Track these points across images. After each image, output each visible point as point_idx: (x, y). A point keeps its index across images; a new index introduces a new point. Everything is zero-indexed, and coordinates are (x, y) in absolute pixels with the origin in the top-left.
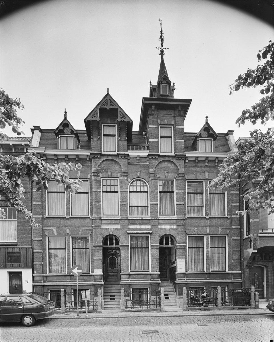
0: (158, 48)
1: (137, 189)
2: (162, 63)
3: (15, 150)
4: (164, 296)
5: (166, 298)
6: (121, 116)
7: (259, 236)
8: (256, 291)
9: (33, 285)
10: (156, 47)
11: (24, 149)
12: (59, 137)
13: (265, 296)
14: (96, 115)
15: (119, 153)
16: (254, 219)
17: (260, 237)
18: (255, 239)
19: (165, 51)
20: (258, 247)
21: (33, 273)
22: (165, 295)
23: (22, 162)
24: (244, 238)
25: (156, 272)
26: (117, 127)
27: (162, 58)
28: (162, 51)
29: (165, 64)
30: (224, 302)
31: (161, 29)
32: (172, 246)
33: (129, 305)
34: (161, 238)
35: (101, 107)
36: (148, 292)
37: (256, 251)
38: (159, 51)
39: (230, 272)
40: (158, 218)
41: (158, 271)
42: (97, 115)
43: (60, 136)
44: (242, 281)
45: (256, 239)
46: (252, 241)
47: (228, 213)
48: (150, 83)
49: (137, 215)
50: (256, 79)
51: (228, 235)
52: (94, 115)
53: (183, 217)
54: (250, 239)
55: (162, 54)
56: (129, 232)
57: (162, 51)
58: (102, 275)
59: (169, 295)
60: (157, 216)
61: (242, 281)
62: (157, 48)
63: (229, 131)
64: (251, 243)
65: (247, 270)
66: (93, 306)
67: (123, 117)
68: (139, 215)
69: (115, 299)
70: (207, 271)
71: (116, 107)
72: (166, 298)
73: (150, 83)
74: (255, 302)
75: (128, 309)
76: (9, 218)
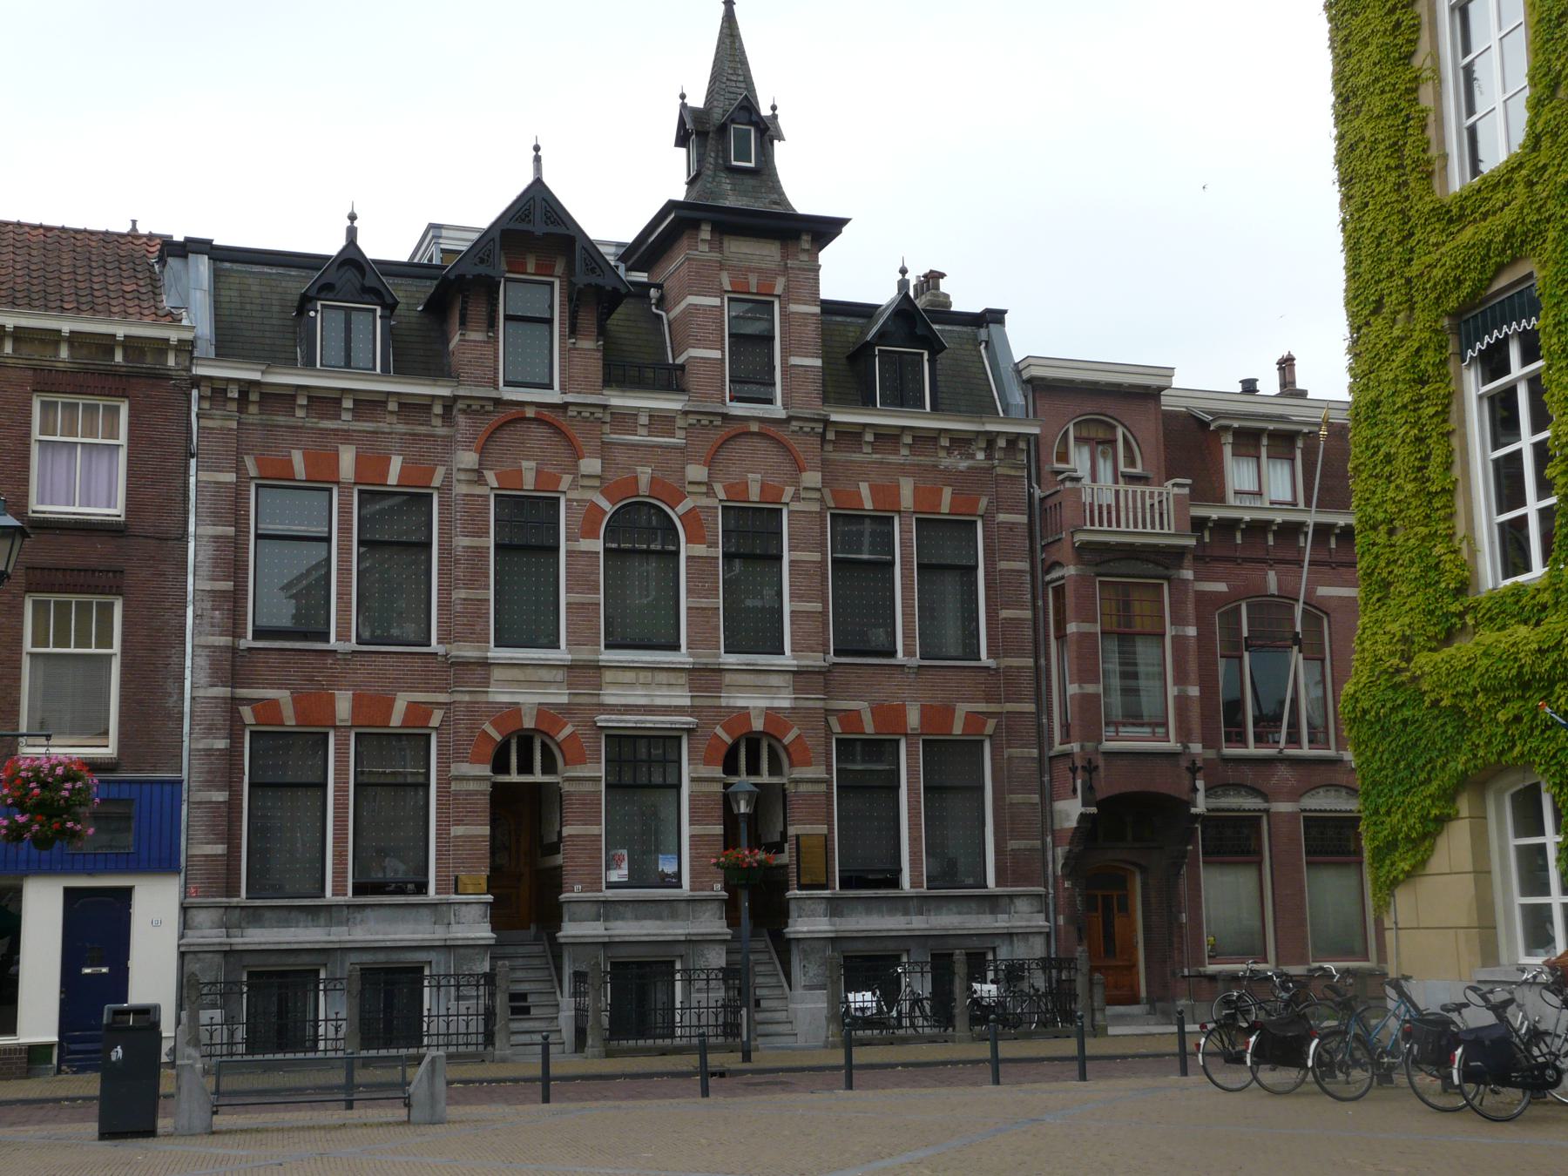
3: (125, 357)
4: (511, 1000)
5: (515, 1011)
7: (1104, 753)
8: (1093, 969)
9: (183, 949)
11: (167, 354)
12: (316, 311)
13: (1143, 993)
14: (488, 256)
15: (569, 398)
16: (1084, 685)
18: (1090, 761)
20: (1100, 796)
21: (186, 894)
22: (514, 997)
24: (1052, 754)
30: (385, 369)
32: (775, 780)
33: (690, 1027)
35: (508, 227)
37: (1093, 810)
39: (1000, 891)
41: (718, 886)
42: (491, 256)
43: (319, 308)
45: (1094, 764)
46: (1079, 771)
48: (683, 96)
52: (481, 255)
53: (818, 663)
54: (1073, 764)
56: (603, 720)
59: (530, 999)
60: (718, 656)
63: (988, 311)
64: (1074, 779)
65: (1067, 885)
67: (593, 270)
69: (533, 1011)
70: (911, 887)
71: (567, 232)
72: (515, 1011)
73: (683, 96)
74: (1093, 1010)
76: (96, 648)
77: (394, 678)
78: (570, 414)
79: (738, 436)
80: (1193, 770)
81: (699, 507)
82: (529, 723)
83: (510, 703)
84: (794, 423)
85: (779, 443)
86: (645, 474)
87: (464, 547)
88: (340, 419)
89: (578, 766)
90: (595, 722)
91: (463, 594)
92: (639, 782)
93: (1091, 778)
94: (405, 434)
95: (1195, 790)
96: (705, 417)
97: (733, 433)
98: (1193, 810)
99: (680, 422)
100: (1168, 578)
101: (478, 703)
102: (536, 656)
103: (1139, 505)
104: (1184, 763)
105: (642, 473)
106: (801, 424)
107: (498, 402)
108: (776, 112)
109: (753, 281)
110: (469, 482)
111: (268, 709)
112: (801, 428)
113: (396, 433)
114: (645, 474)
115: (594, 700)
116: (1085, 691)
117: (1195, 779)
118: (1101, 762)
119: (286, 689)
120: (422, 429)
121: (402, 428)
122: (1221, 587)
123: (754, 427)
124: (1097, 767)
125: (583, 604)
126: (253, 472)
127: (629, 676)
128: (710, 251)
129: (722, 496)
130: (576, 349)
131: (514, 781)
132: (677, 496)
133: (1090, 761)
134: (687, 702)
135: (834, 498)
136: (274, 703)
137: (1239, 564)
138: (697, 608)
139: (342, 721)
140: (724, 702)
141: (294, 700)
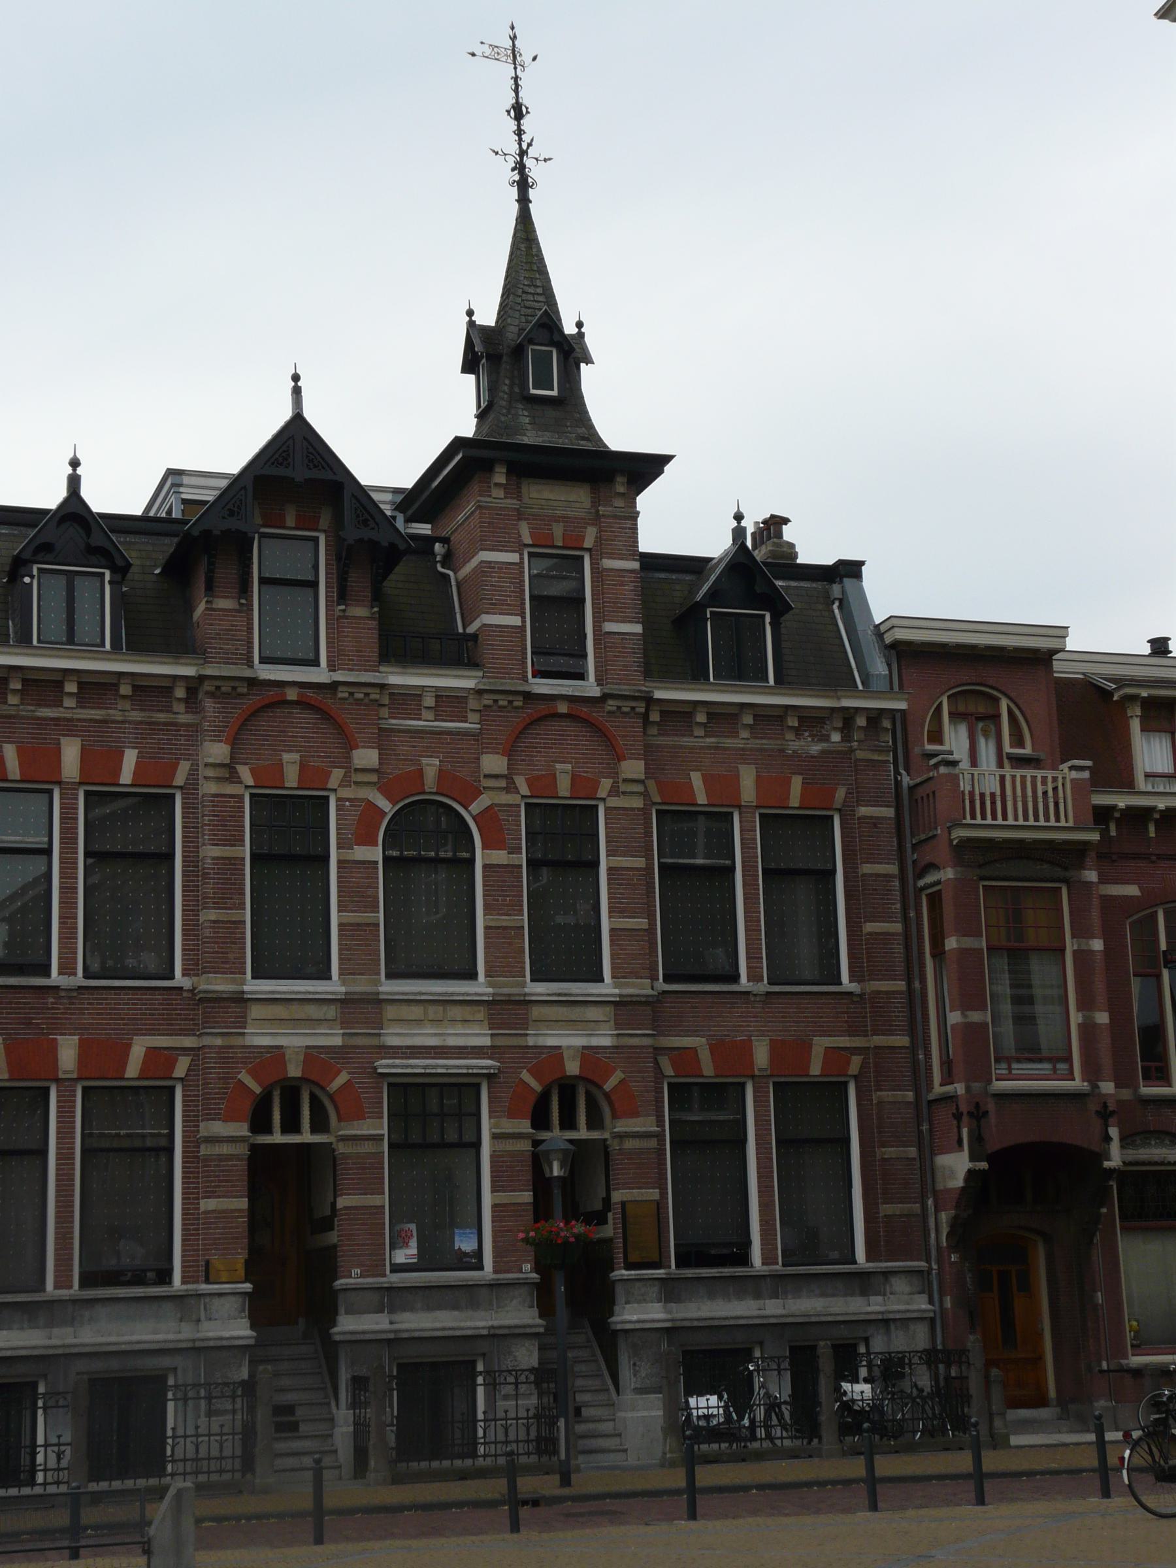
2: (525, 222)
6: (358, 516)
12: (32, 577)
13: (1052, 1393)
14: (239, 507)
15: (339, 676)
17: (1002, 1097)
18: (977, 1105)
19: (534, 170)
24: (931, 1097)
25: (521, 1272)
26: (327, 545)
27: (524, 201)
28: (520, 167)
29: (593, 421)
31: (516, 91)
32: (595, 1135)
36: (36, 1404)
37: (984, 1165)
40: (525, 995)
41: (527, 1267)
43: (35, 572)
44: (934, 1312)
46: (965, 1119)
48: (470, 313)
51: (839, 810)
54: (957, 1108)
55: (523, 185)
56: (385, 1065)
58: (246, 1293)
60: (524, 985)
61: (932, 1315)
62: (497, 153)
64: (959, 1128)
66: (209, 1459)
67: (365, 523)
70: (763, 1264)
73: (470, 313)
75: (900, 1355)
78: (340, 695)
80: (1105, 1115)
81: (496, 805)
84: (610, 702)
86: (431, 766)
92: (919, 1212)
93: (979, 1127)
94: (141, 723)
95: (1108, 1139)
98: (1106, 1164)
99: (473, 703)
100: (1066, 881)
102: (302, 989)
103: (1020, 805)
104: (1093, 1106)
105: (428, 765)
109: (558, 531)
110: (219, 779)
114: (431, 766)
115: (374, 1041)
116: (969, 1020)
117: (1107, 1126)
118: (991, 1106)
120: (162, 717)
121: (136, 715)
122: (1132, 890)
123: (563, 708)
124: (986, 1113)
125: (358, 924)
127: (416, 1012)
129: (524, 790)
130: (347, 617)
132: (470, 793)
133: (977, 1105)
137: (1153, 862)
138: (498, 928)
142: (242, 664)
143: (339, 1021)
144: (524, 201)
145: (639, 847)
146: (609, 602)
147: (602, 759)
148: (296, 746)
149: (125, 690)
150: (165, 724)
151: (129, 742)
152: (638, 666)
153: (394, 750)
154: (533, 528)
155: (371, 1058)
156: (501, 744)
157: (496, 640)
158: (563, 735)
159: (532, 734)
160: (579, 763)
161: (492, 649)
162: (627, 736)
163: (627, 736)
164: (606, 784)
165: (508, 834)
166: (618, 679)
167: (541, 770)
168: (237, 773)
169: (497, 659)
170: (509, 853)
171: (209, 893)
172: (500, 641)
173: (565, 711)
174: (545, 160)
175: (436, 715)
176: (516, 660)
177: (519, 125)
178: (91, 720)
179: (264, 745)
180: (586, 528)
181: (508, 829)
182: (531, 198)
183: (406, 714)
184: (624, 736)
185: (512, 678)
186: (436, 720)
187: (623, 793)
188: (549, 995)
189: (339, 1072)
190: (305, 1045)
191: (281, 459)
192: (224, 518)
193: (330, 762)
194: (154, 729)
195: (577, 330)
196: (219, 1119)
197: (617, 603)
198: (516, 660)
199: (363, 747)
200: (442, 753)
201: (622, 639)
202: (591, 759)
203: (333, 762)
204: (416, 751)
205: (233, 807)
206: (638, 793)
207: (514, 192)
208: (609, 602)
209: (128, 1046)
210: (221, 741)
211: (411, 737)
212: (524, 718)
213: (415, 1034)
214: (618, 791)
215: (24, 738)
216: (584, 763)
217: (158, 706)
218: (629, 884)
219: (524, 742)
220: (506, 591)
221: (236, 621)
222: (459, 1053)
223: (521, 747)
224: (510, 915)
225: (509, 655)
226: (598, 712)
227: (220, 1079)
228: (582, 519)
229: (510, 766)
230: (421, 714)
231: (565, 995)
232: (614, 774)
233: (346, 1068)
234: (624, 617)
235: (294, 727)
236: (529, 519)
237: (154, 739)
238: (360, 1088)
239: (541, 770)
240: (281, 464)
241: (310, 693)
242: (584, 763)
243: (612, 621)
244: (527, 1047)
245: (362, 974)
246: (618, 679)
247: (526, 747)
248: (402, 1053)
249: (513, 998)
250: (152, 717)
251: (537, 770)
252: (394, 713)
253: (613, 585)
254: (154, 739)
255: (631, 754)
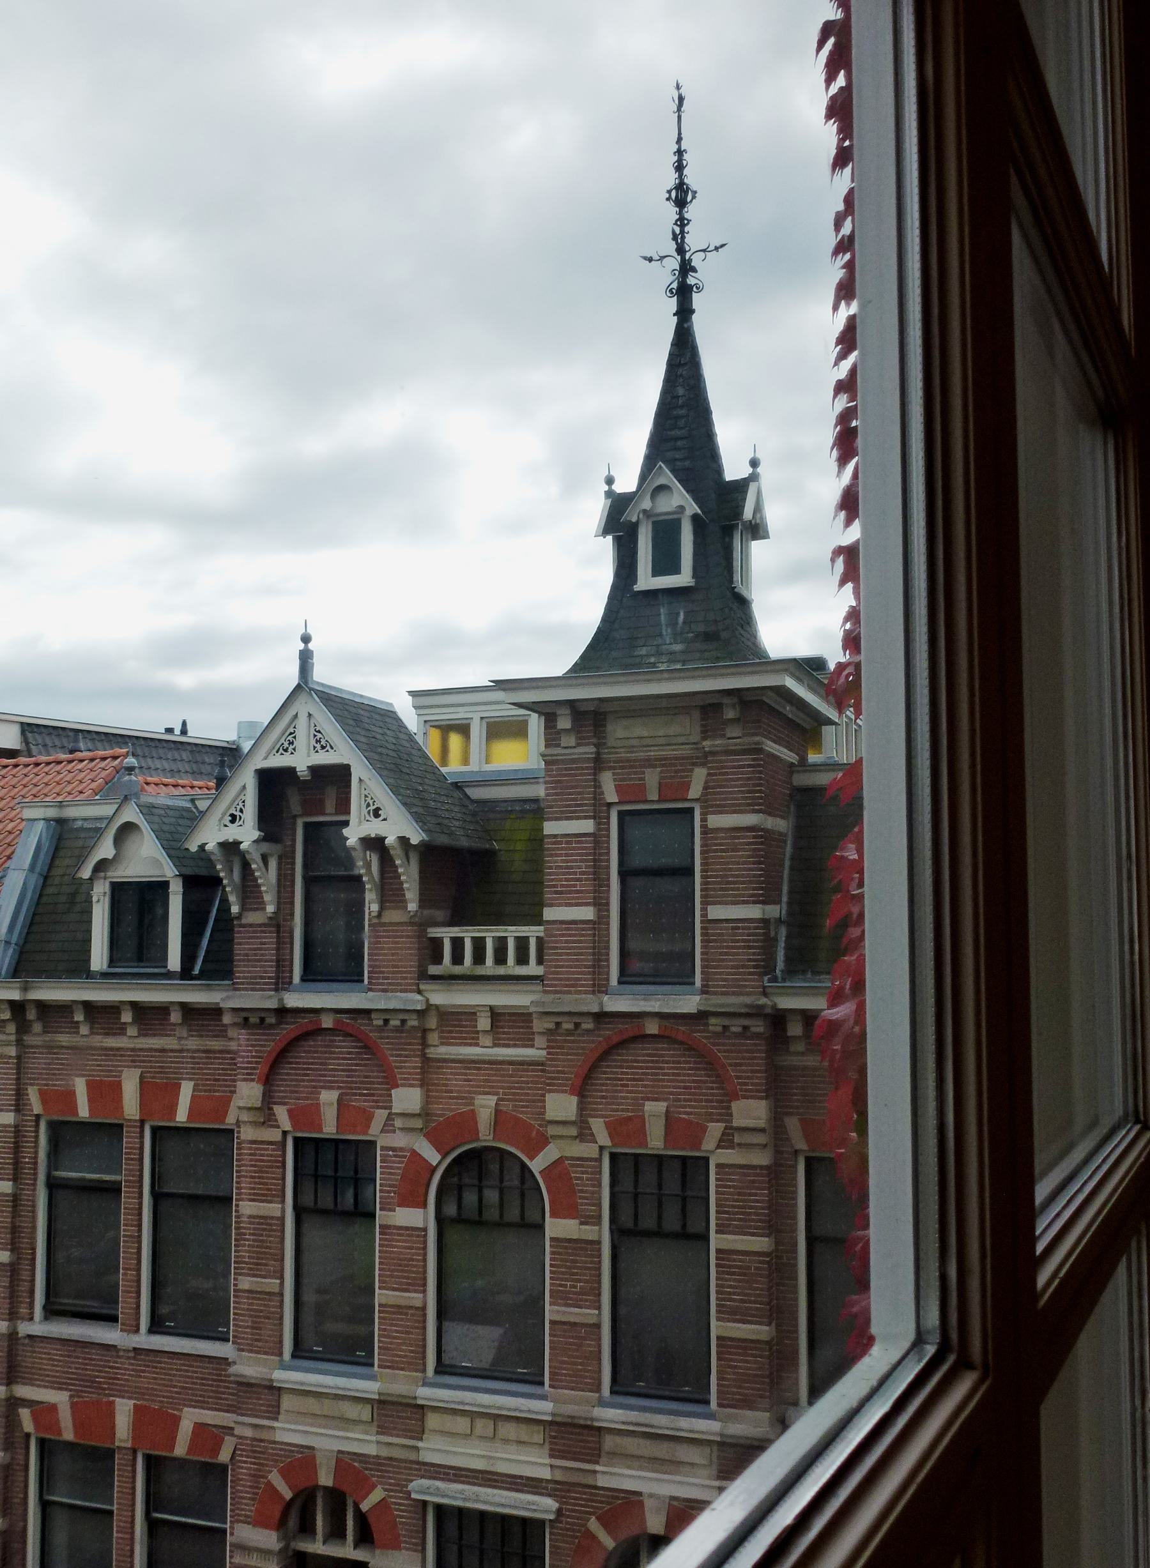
0: (662, 258)
1: (660, 1217)
10: (645, 258)
14: (241, 811)
23: (9, 1230)
27: (684, 312)
31: (680, 167)
34: (281, 1006)
38: (666, 273)
47: (308, 1200)
49: (691, 980)
50: (771, 747)
55: (684, 293)
56: (422, 1488)
57: (686, 268)
62: (650, 260)
68: (113, 1190)
73: (610, 481)
77: (183, 1388)
78: (375, 1022)
79: (623, 1044)
81: (567, 1158)
82: (325, 1479)
83: (302, 1446)
84: (713, 1021)
85: (690, 1048)
86: (485, 1106)
87: (250, 1217)
88: (125, 1034)
89: (390, 1551)
90: (409, 1493)
91: (246, 1283)
94: (198, 1051)
96: (566, 1019)
97: (615, 1040)
99: (538, 1025)
101: (262, 1441)
102: (331, 1384)
105: (482, 1106)
106: (726, 1022)
107: (282, 1012)
108: (311, 646)
109: (652, 779)
110: (255, 1124)
111: (44, 1413)
112: (725, 1028)
113: (188, 1051)
114: (485, 1106)
115: (412, 1456)
119: (66, 1389)
120: (215, 1044)
121: (193, 1043)
123: (652, 1028)
125: (399, 1307)
126: (37, 1108)
127: (462, 1424)
128: (578, 745)
129: (604, 1139)
130: (384, 924)
131: (319, 1552)
132: (538, 1144)
134: (546, 1474)
135: (806, 1136)
136: (53, 1408)
138: (564, 1323)
139: (121, 1441)
140: (602, 1481)
141: (73, 1406)
142: (270, 990)
143: (375, 1423)
144: (684, 312)
145: (760, 1221)
146: (716, 877)
147: (712, 1095)
148: (337, 1082)
149: (175, 1017)
150: (221, 1052)
151: (187, 1073)
152: (755, 967)
153: (446, 1085)
154: (621, 780)
155: (409, 1475)
156: (570, 1079)
157: (561, 942)
158: (657, 1062)
159: (615, 1061)
160: (679, 1100)
161: (556, 954)
162: (741, 1065)
163: (741, 1065)
164: (715, 1130)
165: (581, 1198)
166: (724, 986)
167: (627, 1110)
168: (274, 1115)
169: (562, 966)
170: (582, 1223)
171: (244, 1257)
172: (567, 942)
173: (656, 1032)
174: (717, 249)
175: (494, 1039)
176: (586, 967)
177: (680, 213)
178: (151, 1050)
179: (304, 1081)
180: (692, 771)
181: (582, 1191)
182: (694, 307)
183: (459, 1038)
184: (736, 1065)
185: (580, 992)
186: (495, 1045)
187: (739, 1145)
188: (623, 1423)
189: (373, 1487)
190: (336, 1449)
191: (286, 745)
192: (226, 826)
193: (373, 1101)
194: (210, 1058)
195: (751, 470)
196: (249, 1523)
197: (727, 876)
198: (586, 967)
199: (403, 1085)
200: (502, 1088)
201: (733, 928)
202: (695, 1094)
203: (377, 1101)
204: (470, 1086)
205: (271, 1156)
206: (758, 1145)
207: (672, 304)
208: (716, 877)
209: (176, 1420)
210: (253, 1080)
211: (466, 1068)
212: (600, 1042)
213: (455, 1453)
214: (732, 1141)
215: (94, 1070)
216: (685, 1100)
217: (215, 1031)
218: (745, 1275)
219: (605, 1073)
220: (575, 873)
221: (265, 937)
222: (511, 1483)
223: (600, 1079)
224: (580, 1307)
225: (577, 960)
226: (699, 1031)
227: (250, 1475)
228: (687, 758)
229: (582, 1107)
230: (478, 1038)
231: (646, 1426)
232: (726, 1116)
233: (381, 1483)
234: (735, 896)
235: (335, 1059)
236: (614, 768)
237: (210, 1069)
238: (397, 1510)
239: (627, 1110)
240: (286, 750)
241: (345, 1018)
242: (685, 1100)
243: (720, 903)
244: (596, 1487)
245: (402, 1369)
246: (724, 986)
247: (607, 1079)
248: (444, 1474)
249: (576, 1421)
250: (206, 1045)
251: (623, 1110)
252: (447, 1038)
253: (723, 851)
254: (210, 1069)
255: (746, 1090)
